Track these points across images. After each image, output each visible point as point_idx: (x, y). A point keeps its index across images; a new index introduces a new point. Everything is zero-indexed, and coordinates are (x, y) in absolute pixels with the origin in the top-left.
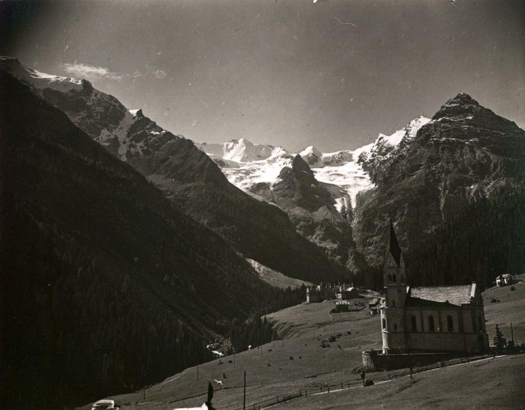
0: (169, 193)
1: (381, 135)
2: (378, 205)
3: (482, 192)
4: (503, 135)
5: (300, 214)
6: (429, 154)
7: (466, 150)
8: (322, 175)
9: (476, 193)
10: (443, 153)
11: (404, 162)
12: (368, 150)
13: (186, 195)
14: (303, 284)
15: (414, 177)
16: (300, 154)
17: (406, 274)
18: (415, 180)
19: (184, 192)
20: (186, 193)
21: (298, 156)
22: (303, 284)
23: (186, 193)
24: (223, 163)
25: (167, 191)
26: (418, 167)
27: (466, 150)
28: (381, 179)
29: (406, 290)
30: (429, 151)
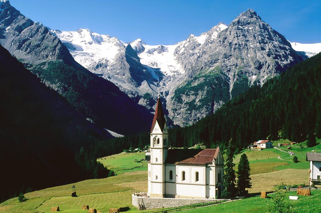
0: (29, 65)
1: (192, 35)
2: (186, 86)
3: (259, 82)
4: (78, 79)
5: (128, 89)
6: (225, 52)
7: (251, 51)
8: (145, 59)
9: (255, 82)
10: (235, 51)
11: (206, 56)
12: (183, 44)
13: (42, 68)
14: (235, 165)
15: (213, 67)
16: (131, 44)
17: (221, 143)
18: (214, 70)
19: (40, 66)
20: (42, 67)
21: (129, 46)
22: (235, 165)
23: (42, 67)
24: (74, 48)
25: (27, 64)
26: (216, 61)
27: (251, 51)
28: (189, 67)
29: (119, 138)
30: (225, 50)
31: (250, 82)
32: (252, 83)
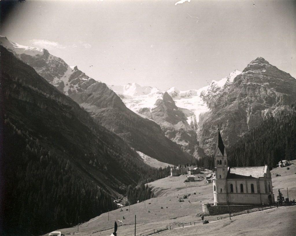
31: (264, 114)
32: (265, 115)
